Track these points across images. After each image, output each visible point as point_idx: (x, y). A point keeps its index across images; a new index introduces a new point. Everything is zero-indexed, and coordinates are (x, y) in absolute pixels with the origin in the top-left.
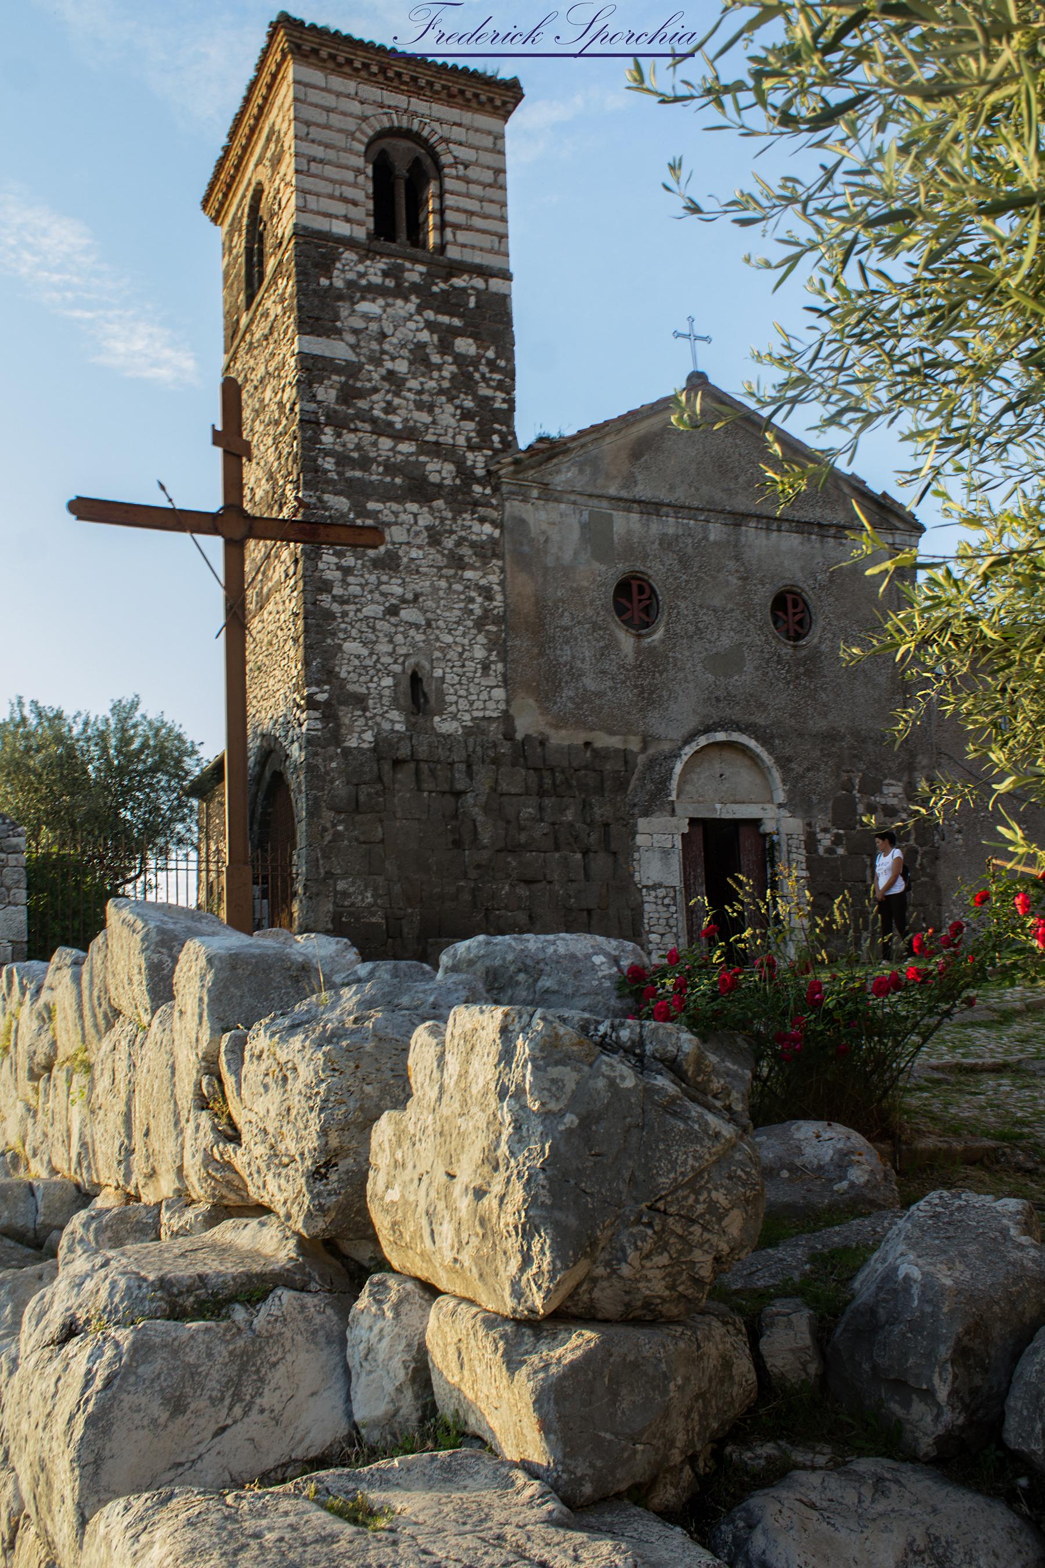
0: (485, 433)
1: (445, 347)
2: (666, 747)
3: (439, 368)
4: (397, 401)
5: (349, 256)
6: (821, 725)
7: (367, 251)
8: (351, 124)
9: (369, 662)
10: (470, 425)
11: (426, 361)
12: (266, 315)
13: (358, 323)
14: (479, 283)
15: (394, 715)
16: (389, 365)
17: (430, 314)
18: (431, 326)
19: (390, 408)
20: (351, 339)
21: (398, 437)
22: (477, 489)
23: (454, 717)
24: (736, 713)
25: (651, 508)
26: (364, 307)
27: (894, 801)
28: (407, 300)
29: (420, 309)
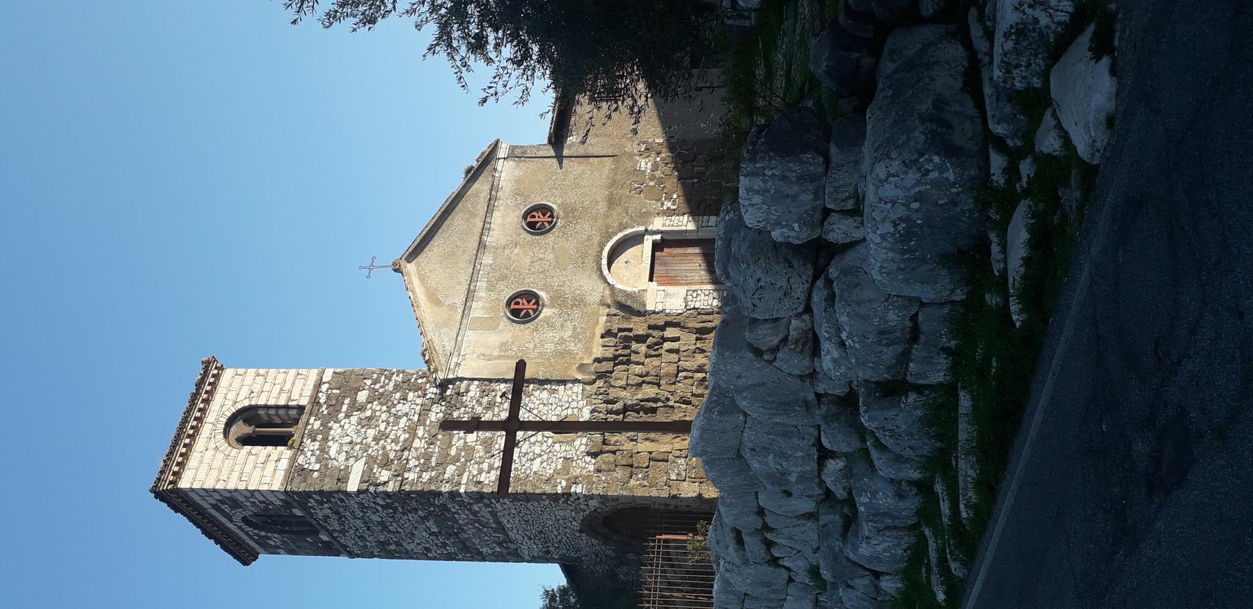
0: (417, 388)
1: (362, 409)
2: (607, 292)
3: (374, 411)
4: (392, 436)
5: (301, 460)
6: (602, 207)
7: (300, 449)
8: (220, 456)
9: (545, 457)
10: (411, 395)
11: (370, 418)
12: (326, 517)
13: (342, 457)
14: (324, 387)
15: (577, 443)
16: (369, 440)
17: (341, 415)
18: (348, 416)
19: (395, 441)
20: (352, 460)
21: (414, 435)
22: (448, 392)
23: (581, 410)
24: (593, 252)
25: (470, 295)
26: (333, 453)
27: (649, 165)
28: (331, 429)
29: (337, 421)
